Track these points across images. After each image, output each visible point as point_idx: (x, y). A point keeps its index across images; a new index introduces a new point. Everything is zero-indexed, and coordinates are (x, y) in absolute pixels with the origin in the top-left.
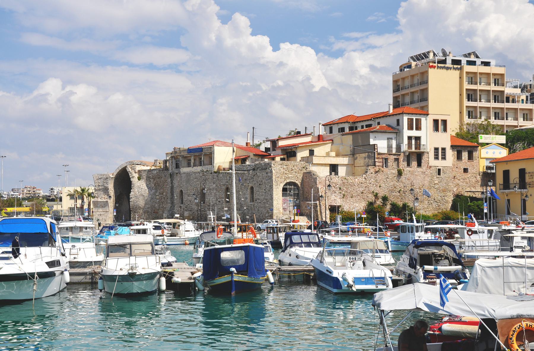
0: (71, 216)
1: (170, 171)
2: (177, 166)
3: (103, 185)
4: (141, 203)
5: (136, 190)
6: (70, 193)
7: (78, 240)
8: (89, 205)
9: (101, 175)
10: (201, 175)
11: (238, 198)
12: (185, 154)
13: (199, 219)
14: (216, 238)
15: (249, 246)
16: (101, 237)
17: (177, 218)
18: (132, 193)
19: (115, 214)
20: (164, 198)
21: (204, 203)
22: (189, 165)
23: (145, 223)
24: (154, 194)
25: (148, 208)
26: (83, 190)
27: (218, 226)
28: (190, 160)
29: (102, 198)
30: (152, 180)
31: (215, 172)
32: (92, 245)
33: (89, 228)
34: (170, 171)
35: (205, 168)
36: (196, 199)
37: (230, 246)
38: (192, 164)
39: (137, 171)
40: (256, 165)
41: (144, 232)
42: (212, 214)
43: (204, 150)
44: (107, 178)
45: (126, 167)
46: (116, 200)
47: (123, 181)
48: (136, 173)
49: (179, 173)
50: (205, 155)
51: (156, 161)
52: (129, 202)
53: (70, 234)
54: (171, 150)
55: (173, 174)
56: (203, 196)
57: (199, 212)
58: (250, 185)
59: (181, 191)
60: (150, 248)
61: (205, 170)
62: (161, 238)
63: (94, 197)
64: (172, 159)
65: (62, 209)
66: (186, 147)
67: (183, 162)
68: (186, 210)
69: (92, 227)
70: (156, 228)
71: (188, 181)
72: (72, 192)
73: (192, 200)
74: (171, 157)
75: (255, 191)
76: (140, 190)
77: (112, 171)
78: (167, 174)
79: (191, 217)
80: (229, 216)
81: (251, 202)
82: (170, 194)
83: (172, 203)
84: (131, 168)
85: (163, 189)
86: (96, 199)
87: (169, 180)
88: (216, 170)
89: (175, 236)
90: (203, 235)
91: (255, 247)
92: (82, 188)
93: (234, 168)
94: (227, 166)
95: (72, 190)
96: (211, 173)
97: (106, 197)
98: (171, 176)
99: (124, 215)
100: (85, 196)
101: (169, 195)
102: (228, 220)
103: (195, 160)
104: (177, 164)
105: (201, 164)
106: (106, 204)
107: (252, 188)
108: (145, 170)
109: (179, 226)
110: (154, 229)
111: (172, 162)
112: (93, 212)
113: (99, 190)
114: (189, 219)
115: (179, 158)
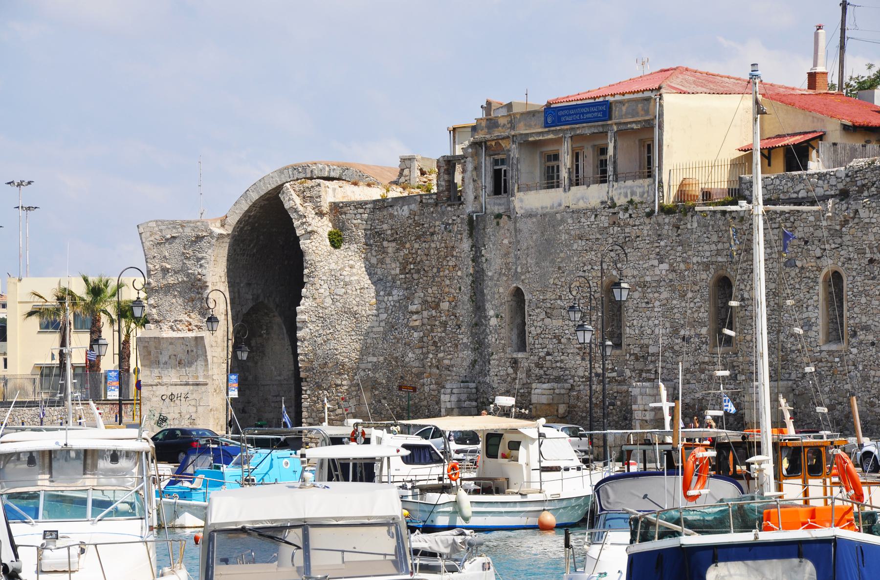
0: (52, 404)
1: (469, 207)
2: (500, 186)
3: (183, 270)
4: (346, 346)
5: (324, 290)
6: (39, 302)
7: (70, 506)
8: (123, 355)
9: (174, 224)
10: (604, 221)
11: (775, 328)
12: (535, 130)
13: (595, 416)
14: (682, 502)
15: (834, 541)
16: (184, 495)
17: (505, 412)
18: (305, 306)
19: (234, 394)
20: (444, 324)
21: (617, 345)
22: (551, 180)
23: (374, 433)
24: (402, 306)
25: (376, 367)
26: (96, 292)
27: (690, 445)
28: (556, 157)
29: (175, 324)
30: (391, 247)
31: (666, 211)
32: (133, 528)
33: (128, 454)
34: (469, 207)
35: (620, 192)
36: (581, 328)
37: (747, 537)
38: (564, 174)
39: (325, 208)
40: (852, 175)
41: (366, 471)
42: (664, 393)
43: (616, 113)
44: (199, 238)
45: (279, 188)
46: (236, 332)
47: (267, 248)
48: (321, 214)
49: (509, 214)
50: (623, 132)
51: (406, 161)
52: (294, 340)
53: (43, 484)
54: (473, 115)
55: (482, 218)
56: (613, 314)
57: (597, 387)
58: (828, 265)
59: (518, 294)
60: (389, 545)
61: (621, 201)
62: (445, 498)
63: (144, 322)
64: (476, 155)
65: (9, 372)
66: (539, 101)
67: (523, 167)
68: (539, 379)
69: (139, 453)
70: (417, 455)
71: (547, 248)
72: (52, 301)
73: (567, 337)
74: (476, 145)
75: (847, 293)
76: (338, 285)
77: (220, 208)
78: (457, 217)
79: (562, 409)
80: (732, 409)
81: (828, 341)
82: (469, 306)
83: (479, 345)
84: (302, 194)
85: (439, 285)
86: (151, 331)
87: (466, 245)
88: (669, 199)
89: (498, 491)
90: (608, 487)
91: (862, 549)
92: (93, 279)
93: (758, 191)
94: (719, 181)
95: (48, 290)
96: (650, 215)
97: (195, 319)
98: (473, 226)
99: (273, 401)
100: (104, 319)
101: (465, 310)
102: (737, 421)
103: (576, 156)
104: (497, 174)
105: (604, 172)
106: (192, 353)
107: (836, 278)
108: (360, 205)
109: (515, 446)
110: (406, 460)
111: (476, 168)
112: (139, 385)
113: (167, 289)
114: (554, 418)
115: (506, 148)
